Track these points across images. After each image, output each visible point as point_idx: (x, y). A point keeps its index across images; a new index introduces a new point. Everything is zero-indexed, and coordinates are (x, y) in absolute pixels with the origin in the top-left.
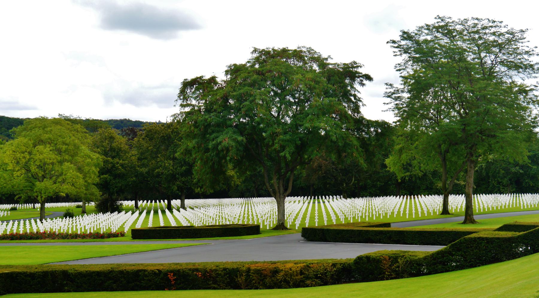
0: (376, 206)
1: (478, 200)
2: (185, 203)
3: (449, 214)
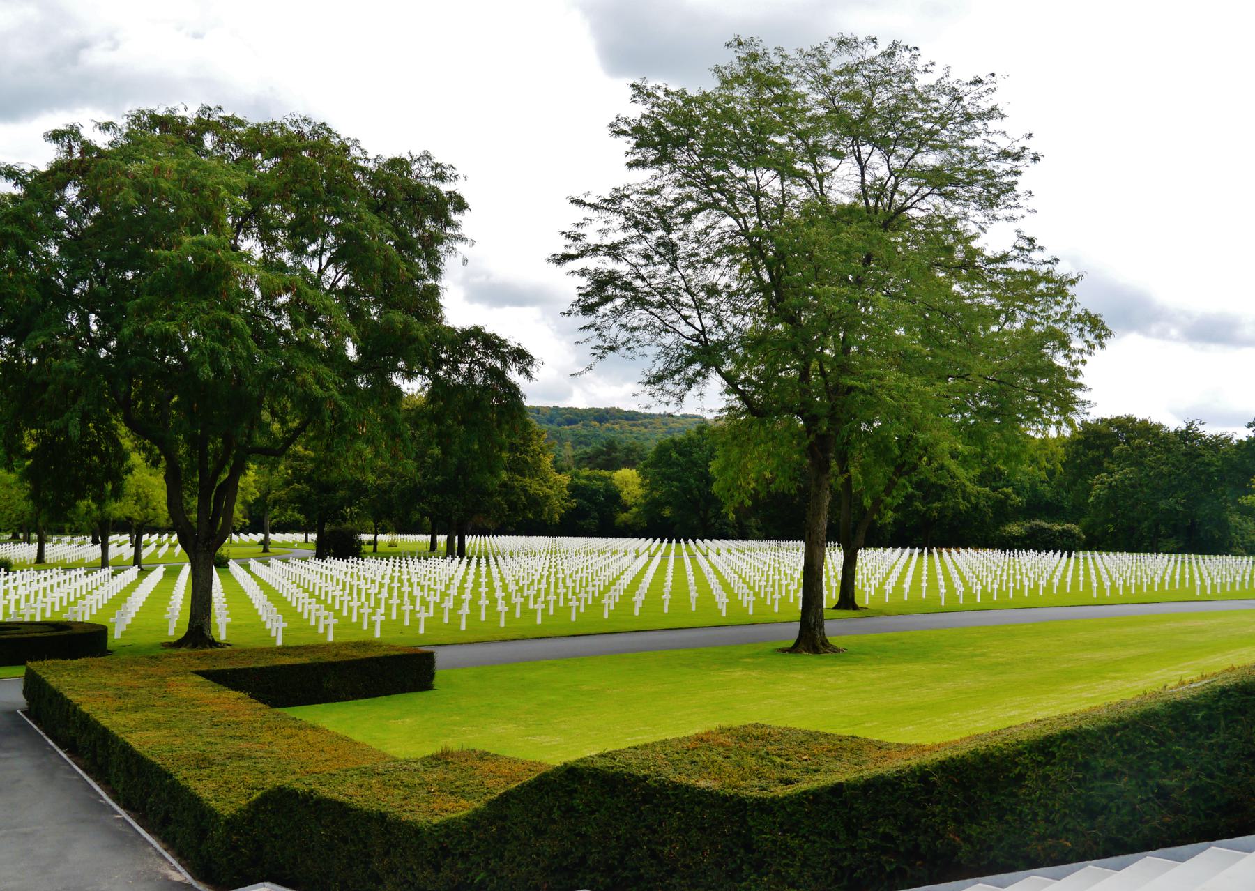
0: (567, 572)
1: (1096, 569)
2: (467, 544)
3: (855, 607)
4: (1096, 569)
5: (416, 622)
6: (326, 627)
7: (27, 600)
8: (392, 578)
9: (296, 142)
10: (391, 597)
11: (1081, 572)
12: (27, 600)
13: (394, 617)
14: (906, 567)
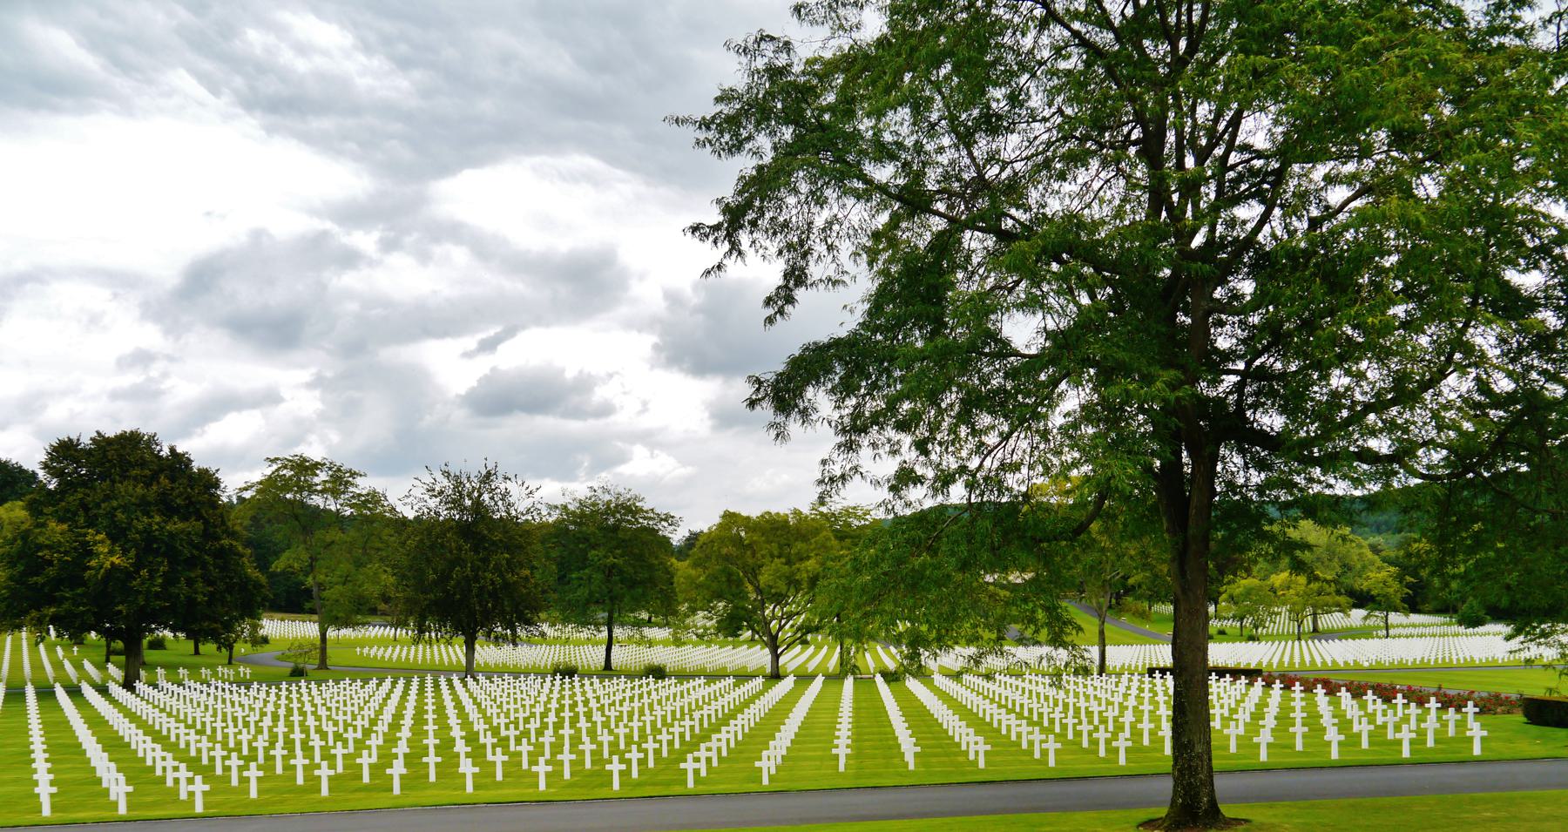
1: (459, 705)
4: (459, 705)
5: (313, 783)
6: (977, 753)
8: (1137, 712)
9: (1076, 515)
10: (272, 744)
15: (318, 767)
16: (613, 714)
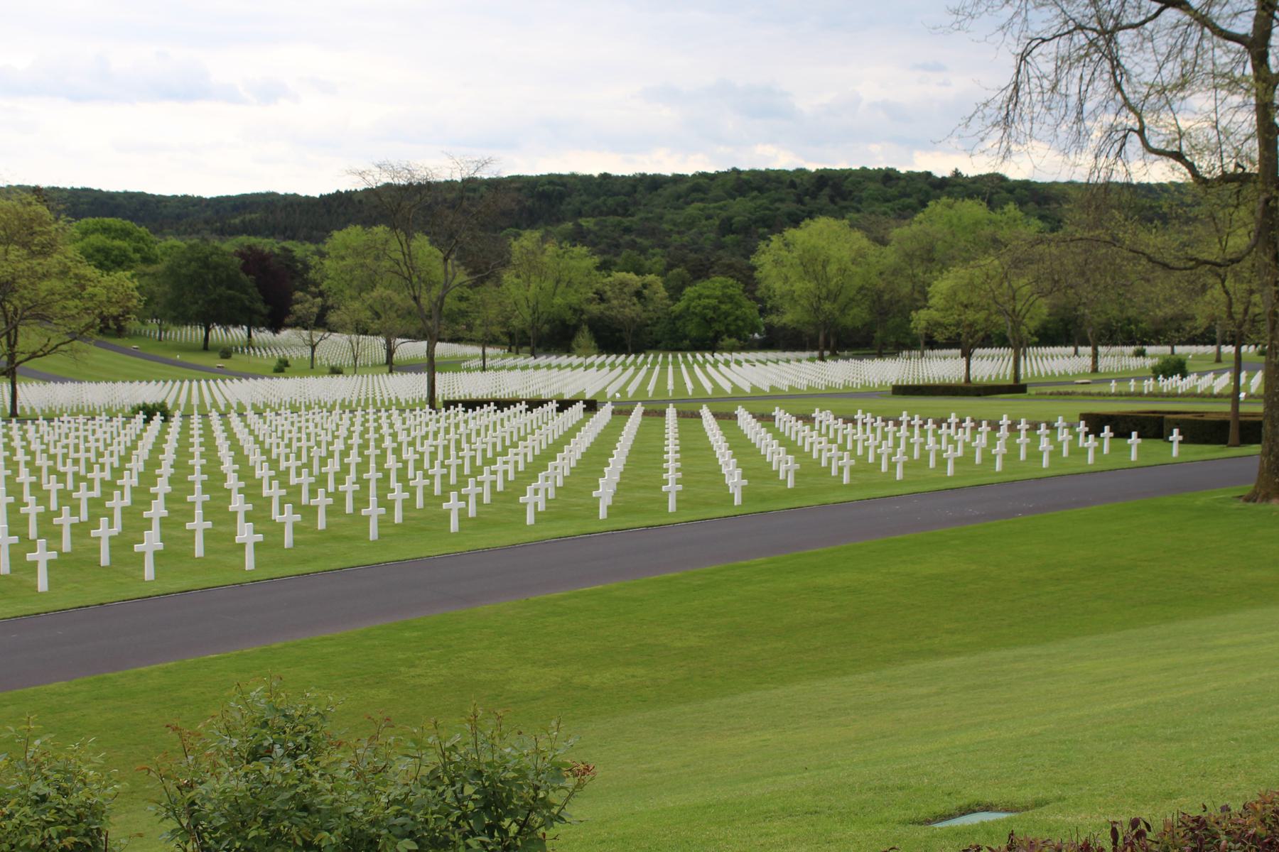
1: (231, 436)
4: (231, 436)
5: (942, 463)
6: (841, 469)
7: (478, 434)
11: (196, 440)
12: (478, 434)
13: (916, 455)
14: (157, 449)
15: (58, 513)
16: (426, 449)
